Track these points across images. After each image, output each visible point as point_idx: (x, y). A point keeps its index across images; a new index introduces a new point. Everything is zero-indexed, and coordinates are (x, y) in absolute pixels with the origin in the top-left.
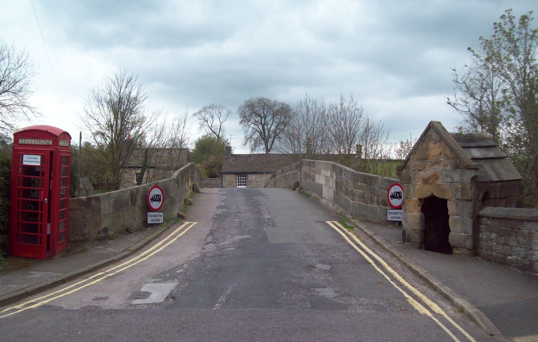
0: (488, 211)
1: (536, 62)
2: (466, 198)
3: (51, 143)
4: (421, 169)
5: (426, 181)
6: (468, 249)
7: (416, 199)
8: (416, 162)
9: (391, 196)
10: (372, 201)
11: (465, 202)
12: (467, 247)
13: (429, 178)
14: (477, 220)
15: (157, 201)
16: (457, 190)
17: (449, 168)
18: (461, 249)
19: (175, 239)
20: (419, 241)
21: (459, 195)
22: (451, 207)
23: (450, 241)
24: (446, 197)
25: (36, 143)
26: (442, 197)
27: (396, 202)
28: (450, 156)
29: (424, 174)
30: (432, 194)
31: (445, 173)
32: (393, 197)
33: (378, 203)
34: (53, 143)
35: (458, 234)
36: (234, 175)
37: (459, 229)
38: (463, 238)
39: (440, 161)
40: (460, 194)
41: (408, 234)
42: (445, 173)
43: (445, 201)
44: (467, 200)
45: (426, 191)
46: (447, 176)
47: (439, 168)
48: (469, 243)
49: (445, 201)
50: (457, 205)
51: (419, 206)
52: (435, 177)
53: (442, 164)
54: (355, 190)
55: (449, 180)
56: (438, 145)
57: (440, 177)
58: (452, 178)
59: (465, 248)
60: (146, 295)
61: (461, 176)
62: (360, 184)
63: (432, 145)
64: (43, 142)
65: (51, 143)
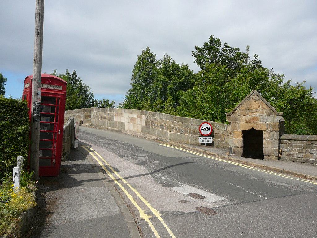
0: (283, 136)
3: (61, 88)
5: (248, 121)
7: (240, 130)
9: (202, 129)
10: (185, 132)
13: (251, 120)
14: (280, 140)
15: (207, 130)
19: (102, 158)
20: (242, 153)
21: (271, 128)
22: (265, 135)
25: (49, 88)
26: (260, 130)
27: (206, 133)
30: (253, 128)
31: (262, 117)
32: (203, 129)
33: (190, 133)
34: (63, 88)
37: (269, 143)
41: (234, 150)
42: (262, 117)
43: (261, 132)
44: (276, 131)
45: (248, 127)
46: (263, 119)
47: (258, 114)
48: (276, 153)
49: (261, 132)
51: (242, 134)
52: (255, 119)
53: (259, 112)
54: (172, 126)
58: (266, 120)
60: (202, 197)
62: (176, 122)
63: (253, 102)
64: (54, 87)
65: (61, 88)
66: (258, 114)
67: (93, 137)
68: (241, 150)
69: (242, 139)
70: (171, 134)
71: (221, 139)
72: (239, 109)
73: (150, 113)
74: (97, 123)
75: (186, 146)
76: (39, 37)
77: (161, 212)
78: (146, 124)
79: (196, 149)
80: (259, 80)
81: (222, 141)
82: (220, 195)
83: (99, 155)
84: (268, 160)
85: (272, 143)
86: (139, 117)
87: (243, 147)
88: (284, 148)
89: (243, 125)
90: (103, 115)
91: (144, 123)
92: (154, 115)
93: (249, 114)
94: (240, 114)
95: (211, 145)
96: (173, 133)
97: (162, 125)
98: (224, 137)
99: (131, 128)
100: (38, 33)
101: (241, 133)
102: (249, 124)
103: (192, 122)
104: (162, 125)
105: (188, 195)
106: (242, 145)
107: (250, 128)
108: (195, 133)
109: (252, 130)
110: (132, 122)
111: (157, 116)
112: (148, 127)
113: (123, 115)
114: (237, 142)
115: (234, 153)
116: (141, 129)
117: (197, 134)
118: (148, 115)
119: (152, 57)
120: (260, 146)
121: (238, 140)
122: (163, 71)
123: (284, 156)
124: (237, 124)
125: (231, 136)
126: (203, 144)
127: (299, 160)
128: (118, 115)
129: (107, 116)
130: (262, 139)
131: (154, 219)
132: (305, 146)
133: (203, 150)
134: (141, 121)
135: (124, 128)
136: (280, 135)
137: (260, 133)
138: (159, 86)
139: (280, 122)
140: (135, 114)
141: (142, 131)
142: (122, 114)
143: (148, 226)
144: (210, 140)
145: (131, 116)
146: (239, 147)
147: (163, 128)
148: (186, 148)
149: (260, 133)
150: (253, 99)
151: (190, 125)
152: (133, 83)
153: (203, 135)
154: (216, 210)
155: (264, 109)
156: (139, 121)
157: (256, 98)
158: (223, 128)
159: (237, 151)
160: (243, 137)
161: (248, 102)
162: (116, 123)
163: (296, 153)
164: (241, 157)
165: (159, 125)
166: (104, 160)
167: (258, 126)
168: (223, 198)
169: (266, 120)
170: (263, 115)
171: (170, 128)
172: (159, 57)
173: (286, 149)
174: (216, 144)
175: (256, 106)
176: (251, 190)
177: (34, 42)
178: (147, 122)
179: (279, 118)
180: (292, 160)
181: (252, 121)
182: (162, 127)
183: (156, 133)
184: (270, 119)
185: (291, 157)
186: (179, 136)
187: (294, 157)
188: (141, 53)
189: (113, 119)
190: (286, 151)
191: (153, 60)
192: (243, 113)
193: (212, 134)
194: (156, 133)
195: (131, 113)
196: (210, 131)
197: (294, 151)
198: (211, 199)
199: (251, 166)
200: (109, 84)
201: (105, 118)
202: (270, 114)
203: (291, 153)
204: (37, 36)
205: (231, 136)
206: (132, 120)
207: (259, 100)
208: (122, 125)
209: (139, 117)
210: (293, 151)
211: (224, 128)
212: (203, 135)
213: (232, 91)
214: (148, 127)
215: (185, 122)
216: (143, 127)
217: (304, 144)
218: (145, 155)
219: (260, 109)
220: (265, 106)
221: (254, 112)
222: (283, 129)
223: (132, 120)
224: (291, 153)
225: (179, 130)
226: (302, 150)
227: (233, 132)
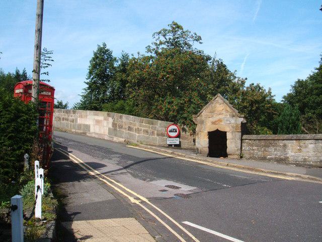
0: (245, 137)
5: (214, 123)
7: (206, 132)
10: (153, 133)
14: (242, 140)
20: (208, 153)
22: (229, 136)
24: (226, 131)
32: (171, 131)
33: (158, 135)
37: (232, 144)
42: (226, 119)
43: (226, 132)
45: (213, 128)
46: (227, 120)
47: (221, 117)
49: (226, 132)
52: (220, 120)
55: (228, 122)
60: (177, 188)
63: (218, 105)
66: (221, 117)
67: (61, 139)
68: (207, 150)
69: (207, 140)
70: (139, 136)
72: (205, 112)
73: (116, 115)
74: (59, 126)
75: (154, 148)
76: (38, 50)
77: (147, 198)
78: (113, 126)
79: (164, 150)
80: (220, 81)
82: (191, 185)
83: (74, 156)
85: (235, 142)
86: (105, 119)
87: (209, 148)
88: (246, 147)
90: (66, 117)
91: (110, 126)
92: (121, 117)
95: (178, 146)
96: (144, 134)
97: (129, 127)
99: (97, 131)
100: (38, 47)
101: (207, 134)
103: (160, 125)
104: (129, 127)
105: (166, 186)
106: (208, 145)
107: (216, 129)
108: (163, 135)
109: (217, 130)
110: (99, 125)
111: (124, 118)
112: (115, 130)
113: (88, 117)
114: (203, 142)
115: (201, 153)
116: (107, 131)
117: (164, 136)
118: (115, 117)
120: (225, 146)
122: (122, 68)
123: (246, 155)
126: (170, 146)
128: (83, 117)
129: (70, 118)
130: (226, 139)
131: (142, 202)
133: (171, 151)
134: (108, 123)
135: (90, 131)
136: (242, 136)
137: (225, 134)
138: (114, 85)
139: (242, 123)
140: (101, 116)
141: (109, 133)
142: (87, 116)
143: (140, 206)
144: (177, 141)
145: (97, 118)
147: (130, 131)
148: (156, 150)
149: (225, 134)
150: (218, 102)
151: (157, 127)
152: (88, 81)
153: (170, 137)
154: (191, 195)
155: (227, 111)
156: (105, 123)
157: (220, 101)
161: (213, 105)
162: (81, 125)
165: (127, 127)
166: (79, 160)
167: (222, 127)
168: (195, 188)
171: (138, 130)
172: (117, 54)
174: (183, 146)
176: (217, 181)
178: (114, 125)
179: (241, 120)
180: (252, 158)
182: (130, 129)
183: (123, 136)
184: (233, 121)
186: (148, 138)
188: (96, 50)
189: (76, 121)
191: (110, 55)
193: (178, 136)
194: (123, 136)
195: (95, 115)
196: (177, 133)
198: (185, 189)
199: (218, 164)
200: (69, 84)
201: (67, 120)
202: (233, 116)
204: (37, 49)
206: (98, 122)
208: (88, 127)
209: (105, 119)
210: (253, 150)
212: (170, 137)
214: (115, 130)
215: (152, 124)
216: (109, 129)
217: (263, 143)
218: (118, 156)
219: (224, 112)
220: (228, 109)
221: (219, 115)
222: (245, 130)
223: (98, 122)
225: (147, 132)
226: (261, 149)
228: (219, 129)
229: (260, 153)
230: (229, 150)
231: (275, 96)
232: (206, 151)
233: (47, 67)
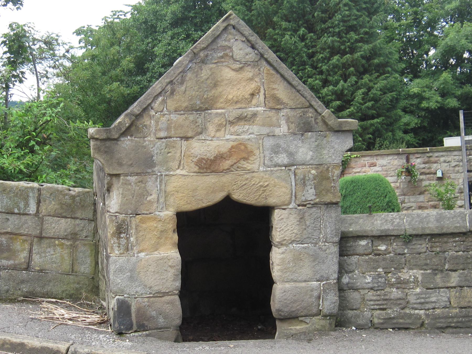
1: (141, 2)
2: (328, 198)
4: (189, 135)
5: (208, 166)
6: (325, 316)
7: (168, 214)
8: (174, 117)
11: (323, 207)
12: (325, 311)
13: (220, 157)
16: (303, 182)
17: (283, 129)
18: (308, 320)
20: (178, 321)
21: (310, 194)
22: (283, 226)
23: (274, 316)
24: (271, 201)
28: (285, 100)
29: (202, 148)
31: (269, 142)
35: (303, 284)
36: (28, 261)
38: (316, 294)
39: (255, 115)
40: (312, 191)
41: (138, 310)
42: (269, 142)
45: (201, 192)
46: (276, 150)
47: (249, 133)
50: (302, 219)
52: (241, 152)
55: (283, 159)
56: (248, 73)
57: (257, 152)
58: (291, 154)
59: (319, 313)
61: (318, 148)
63: (227, 73)
68: (173, 309)
69: (174, 255)
71: (8, 259)
81: (14, 268)
84: (294, 336)
85: (315, 258)
87: (185, 293)
89: (186, 187)
93: (211, 129)
94: (162, 134)
98: (27, 246)
101: (172, 225)
102: (210, 180)
106: (178, 284)
109: (228, 201)
114: (150, 266)
115: (141, 327)
119: (15, 4)
121: (162, 259)
124: (152, 185)
125: (123, 241)
127: (436, 318)
132: (457, 257)
146: (165, 294)
155: (275, 104)
157: (240, 50)
158: (22, 205)
159: (154, 313)
160: (182, 247)
161: (205, 73)
163: (418, 290)
164: (176, 341)
169: (291, 154)
170: (277, 131)
173: (369, 279)
175: (245, 90)
177: (207, 177)
181: (226, 164)
184: (304, 151)
185: (392, 312)
187: (407, 311)
190: (370, 285)
192: (181, 126)
197: (407, 282)
202: (305, 128)
203: (395, 293)
205: (123, 241)
207: (255, 64)
211: (27, 205)
213: (179, 46)
219: (258, 107)
220: (281, 91)
224: (395, 293)
227: (135, 221)
228: (238, 196)
229: (440, 298)
230: (282, 293)
231: (26, 79)
232: (167, 308)
233: (33, 73)
